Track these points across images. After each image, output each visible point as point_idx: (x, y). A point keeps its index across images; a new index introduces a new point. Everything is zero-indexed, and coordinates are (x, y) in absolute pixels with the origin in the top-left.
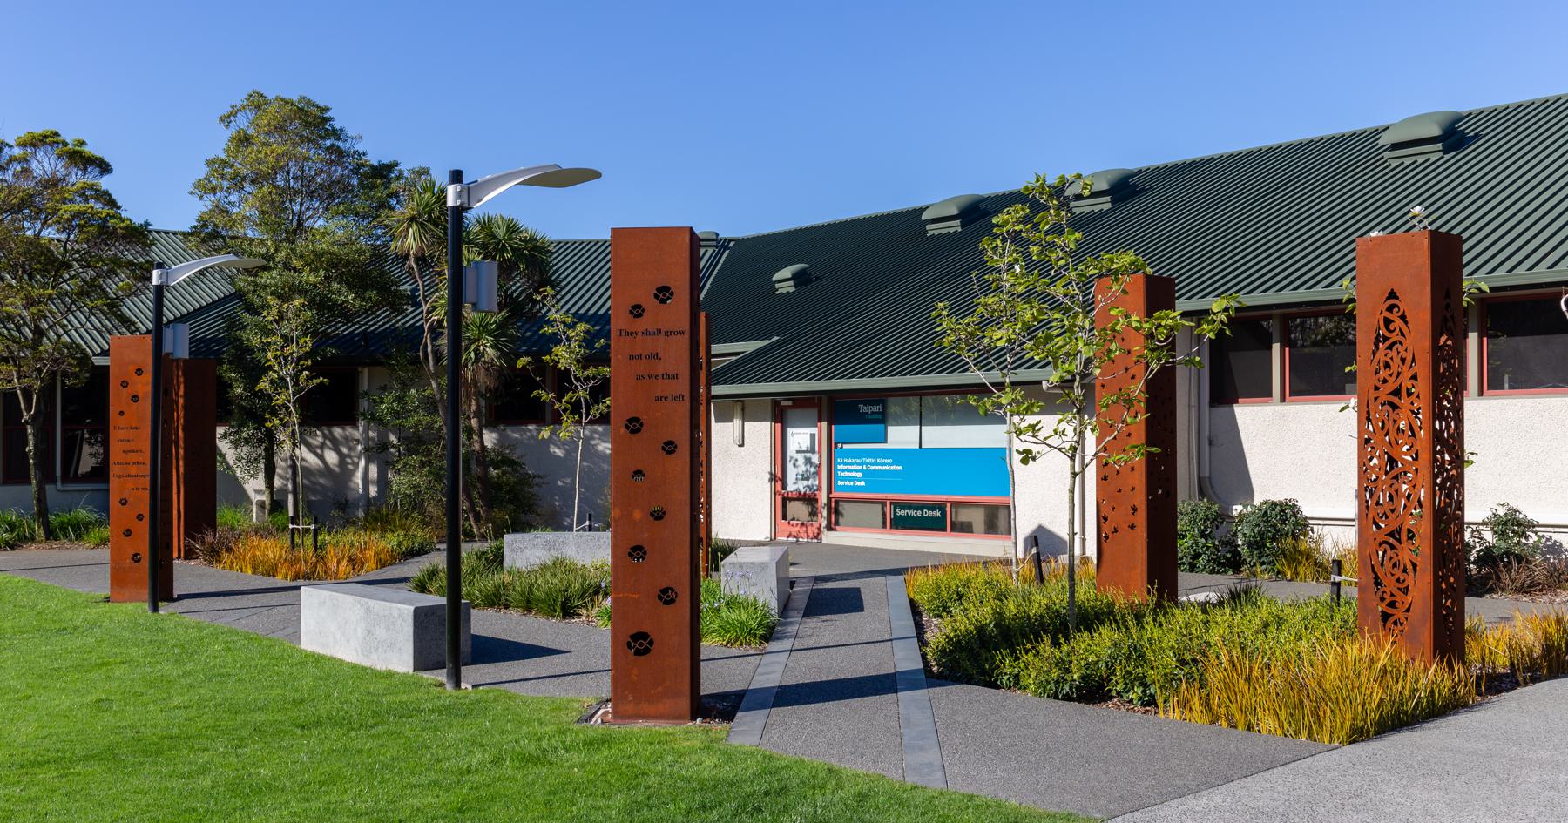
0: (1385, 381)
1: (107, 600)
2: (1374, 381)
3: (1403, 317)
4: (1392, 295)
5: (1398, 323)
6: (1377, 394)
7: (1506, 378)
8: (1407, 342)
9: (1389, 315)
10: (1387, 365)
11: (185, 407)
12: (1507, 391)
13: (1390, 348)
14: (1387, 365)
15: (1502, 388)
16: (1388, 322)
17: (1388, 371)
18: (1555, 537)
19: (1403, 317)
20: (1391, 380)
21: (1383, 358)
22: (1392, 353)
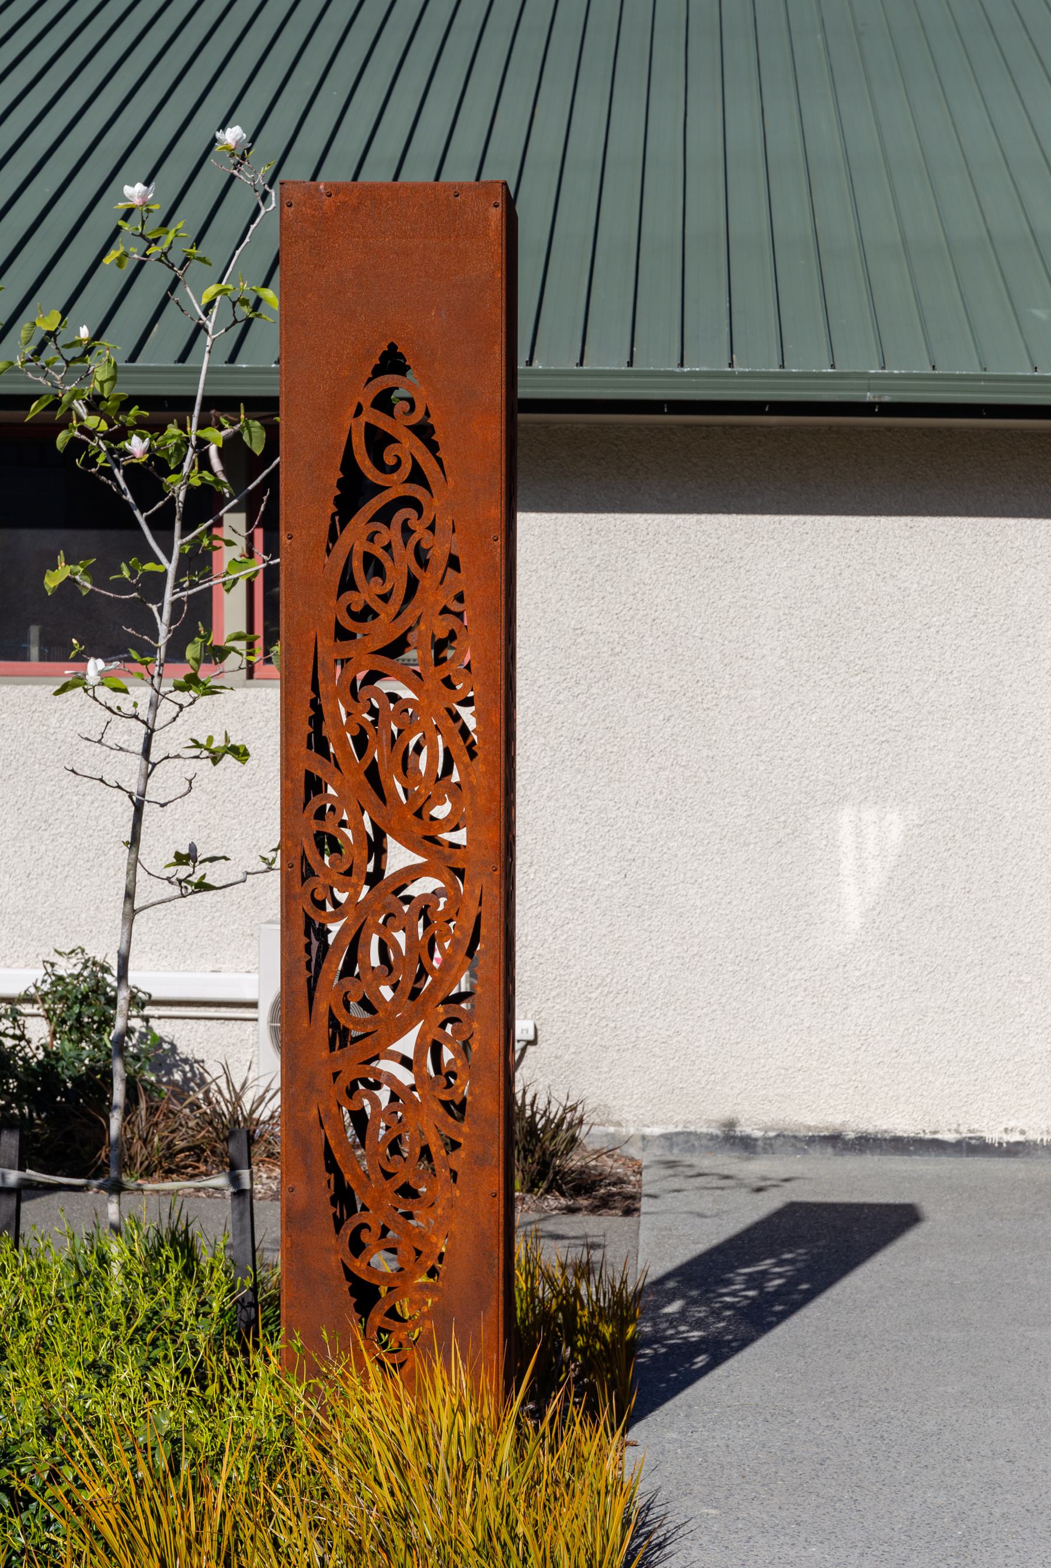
0: (366, 614)
1: (433, 636)
2: (333, 610)
3: (424, 432)
4: (392, 362)
5: (407, 448)
6: (348, 648)
7: (34, 631)
8: (435, 505)
9: (382, 422)
10: (374, 566)
11: (516, 1309)
12: (34, 664)
13: (384, 516)
14: (374, 566)
15: (25, 657)
16: (378, 441)
17: (377, 586)
18: (160, 1028)
19: (424, 432)
20: (386, 612)
21: (361, 547)
22: (392, 534)
